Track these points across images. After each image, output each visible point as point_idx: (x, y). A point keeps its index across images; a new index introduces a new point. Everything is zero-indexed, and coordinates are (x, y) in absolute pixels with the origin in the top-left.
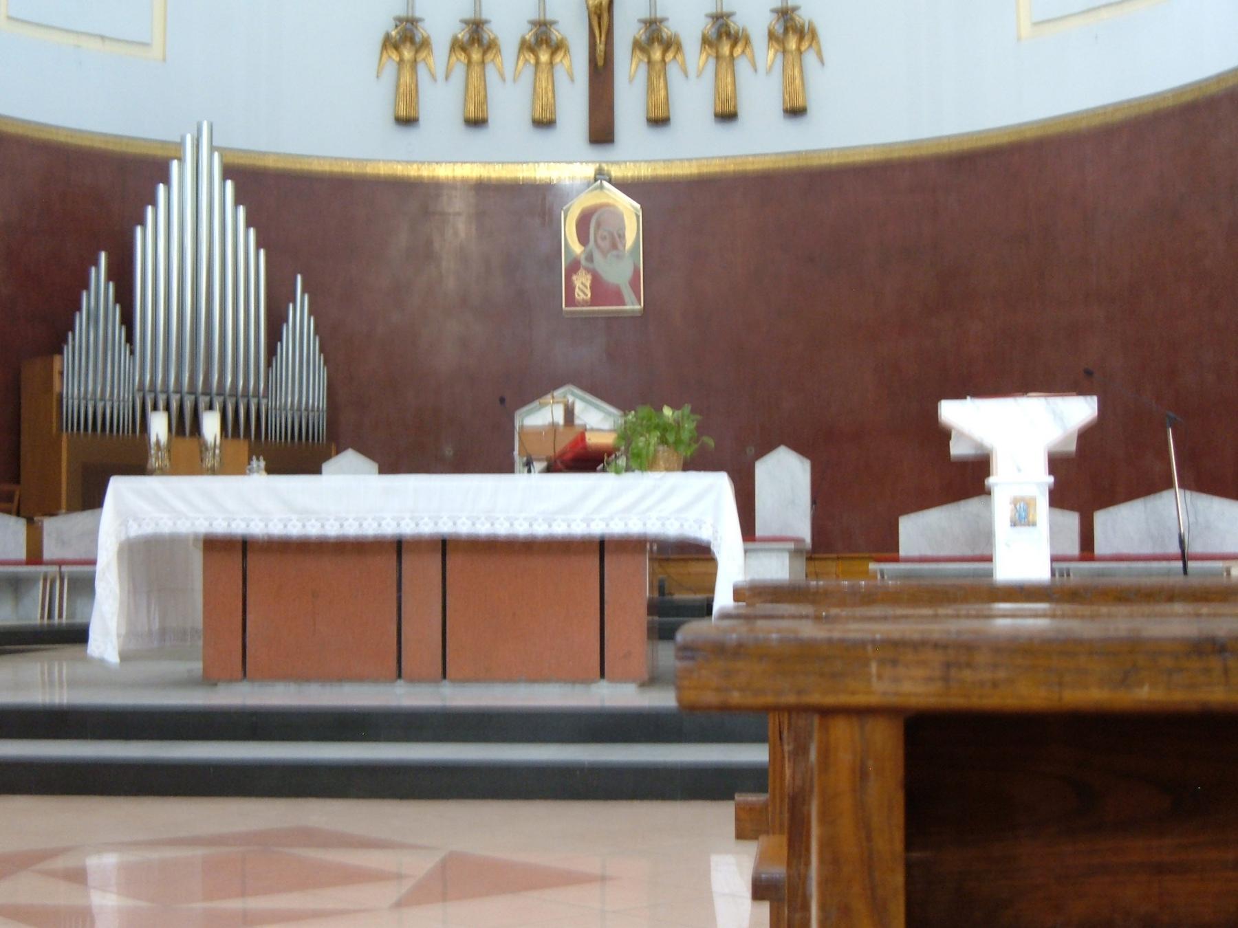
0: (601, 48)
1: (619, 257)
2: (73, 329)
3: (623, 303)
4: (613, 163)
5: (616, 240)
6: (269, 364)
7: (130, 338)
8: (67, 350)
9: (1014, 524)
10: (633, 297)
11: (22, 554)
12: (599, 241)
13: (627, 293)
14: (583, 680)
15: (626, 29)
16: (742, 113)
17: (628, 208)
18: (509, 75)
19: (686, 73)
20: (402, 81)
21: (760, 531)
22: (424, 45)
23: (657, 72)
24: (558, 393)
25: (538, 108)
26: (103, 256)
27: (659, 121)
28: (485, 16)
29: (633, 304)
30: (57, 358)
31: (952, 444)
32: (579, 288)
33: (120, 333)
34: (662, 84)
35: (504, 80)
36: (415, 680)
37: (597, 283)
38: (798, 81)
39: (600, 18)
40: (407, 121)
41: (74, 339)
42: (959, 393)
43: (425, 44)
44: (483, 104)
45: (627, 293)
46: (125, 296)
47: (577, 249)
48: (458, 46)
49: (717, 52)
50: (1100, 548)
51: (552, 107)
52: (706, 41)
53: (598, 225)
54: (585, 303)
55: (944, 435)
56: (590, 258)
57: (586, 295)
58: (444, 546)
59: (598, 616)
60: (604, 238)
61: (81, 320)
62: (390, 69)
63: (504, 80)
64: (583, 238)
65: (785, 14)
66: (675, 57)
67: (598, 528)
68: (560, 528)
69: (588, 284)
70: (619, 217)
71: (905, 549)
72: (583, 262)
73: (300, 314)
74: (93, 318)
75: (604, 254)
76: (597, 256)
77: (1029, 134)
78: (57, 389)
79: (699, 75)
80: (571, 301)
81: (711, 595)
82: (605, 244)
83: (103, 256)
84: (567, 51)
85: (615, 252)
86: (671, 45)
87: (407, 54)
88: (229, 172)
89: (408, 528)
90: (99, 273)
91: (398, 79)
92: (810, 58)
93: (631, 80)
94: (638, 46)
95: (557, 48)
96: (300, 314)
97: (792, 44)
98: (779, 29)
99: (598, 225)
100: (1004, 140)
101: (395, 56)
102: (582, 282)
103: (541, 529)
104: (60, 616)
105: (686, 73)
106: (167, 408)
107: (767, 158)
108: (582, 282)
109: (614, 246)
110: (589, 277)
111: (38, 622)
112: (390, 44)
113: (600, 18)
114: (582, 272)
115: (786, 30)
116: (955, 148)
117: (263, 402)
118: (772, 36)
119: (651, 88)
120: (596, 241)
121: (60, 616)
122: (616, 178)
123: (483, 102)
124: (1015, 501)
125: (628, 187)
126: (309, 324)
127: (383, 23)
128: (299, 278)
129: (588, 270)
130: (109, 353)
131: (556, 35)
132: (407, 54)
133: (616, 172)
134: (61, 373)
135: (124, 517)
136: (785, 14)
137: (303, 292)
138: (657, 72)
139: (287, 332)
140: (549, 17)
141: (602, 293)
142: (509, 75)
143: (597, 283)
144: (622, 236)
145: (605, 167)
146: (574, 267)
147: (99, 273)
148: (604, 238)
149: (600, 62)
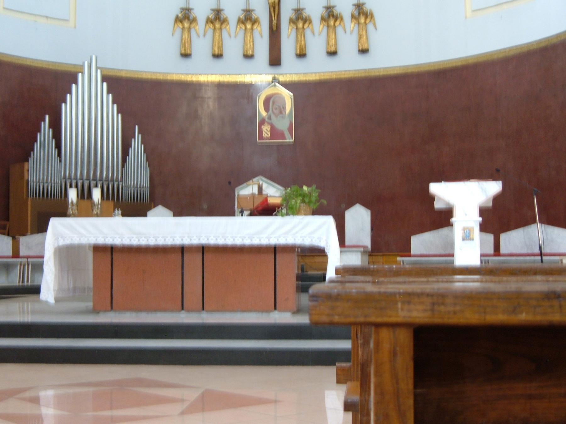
0: (275, 22)
1: (283, 117)
2: (33, 150)
3: (285, 139)
4: (280, 74)
5: (281, 110)
6: (123, 166)
7: (59, 155)
8: (31, 160)
9: (464, 239)
10: (290, 136)
11: (10, 253)
12: (274, 110)
13: (287, 134)
14: (267, 310)
15: (286, 13)
16: (339, 52)
17: (287, 95)
18: (233, 34)
19: (313, 34)
20: (184, 37)
21: (347, 243)
22: (194, 20)
23: (300, 33)
24: (255, 179)
25: (246, 49)
26: (47, 117)
27: (301, 55)
28: (222, 7)
29: (289, 139)
30: (26, 164)
31: (435, 203)
32: (265, 132)
33: (55, 152)
34: (303, 39)
35: (230, 36)
36: (190, 311)
37: (273, 130)
38: (365, 37)
39: (274, 8)
40: (186, 55)
41: (34, 155)
42: (438, 180)
43: (194, 20)
44: (221, 47)
45: (287, 134)
46: (57, 135)
47: (264, 114)
48: (209, 21)
49: (328, 24)
50: (503, 250)
51: (252, 49)
52: (323, 19)
53: (274, 103)
54: (267, 139)
55: (431, 199)
56: (270, 118)
57: (268, 135)
58: (203, 249)
59: (274, 281)
60: (276, 109)
61: (37, 146)
62: (178, 32)
63: (230, 36)
64: (267, 109)
65: (359, 7)
66: (308, 26)
67: (273, 241)
68: (256, 241)
69: (269, 130)
70: (283, 99)
71: (414, 251)
72: (267, 120)
73: (137, 143)
74: (42, 145)
75: (276, 116)
76: (273, 117)
77: (471, 61)
78: (26, 178)
79: (320, 34)
80: (261, 137)
81: (325, 272)
82: (277, 112)
83: (47, 117)
84: (259, 23)
85: (281, 115)
86: (307, 20)
87: (186, 25)
88: (105, 79)
89: (186, 241)
90: (45, 125)
91: (182, 36)
92: (370, 27)
93: (289, 36)
94: (291, 21)
95: (255, 22)
96: (137, 143)
97: (362, 20)
98: (356, 13)
99: (274, 103)
100: (459, 64)
101: (181, 26)
102: (266, 129)
103: (247, 242)
104: (28, 281)
105: (313, 34)
106: (77, 186)
107: (351, 72)
108: (266, 129)
109: (281, 112)
110: (269, 127)
111: (17, 284)
112: (178, 20)
113: (274, 8)
114: (266, 124)
115: (359, 14)
116: (436, 67)
117: (120, 184)
118: (353, 16)
119: (297, 40)
120: (272, 110)
121: (28, 281)
122: (282, 82)
123: (221, 47)
124: (464, 229)
125: (287, 85)
126: (141, 148)
127: (175, 11)
128: (137, 127)
129: (269, 123)
130: (50, 161)
131: (254, 16)
132: (186, 25)
133: (282, 79)
134: (28, 171)
135: (57, 236)
136: (359, 7)
137: (139, 133)
138: (300, 33)
139: (131, 152)
140: (251, 8)
141: (275, 134)
142: (233, 34)
143: (273, 130)
144: (284, 108)
145: (277, 76)
146: (262, 122)
147: (45, 125)
148: (276, 109)
149: (275, 29)
